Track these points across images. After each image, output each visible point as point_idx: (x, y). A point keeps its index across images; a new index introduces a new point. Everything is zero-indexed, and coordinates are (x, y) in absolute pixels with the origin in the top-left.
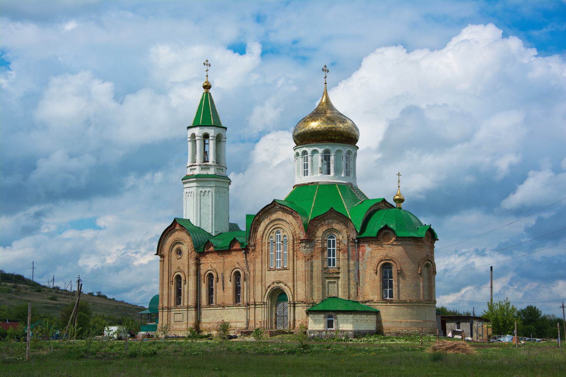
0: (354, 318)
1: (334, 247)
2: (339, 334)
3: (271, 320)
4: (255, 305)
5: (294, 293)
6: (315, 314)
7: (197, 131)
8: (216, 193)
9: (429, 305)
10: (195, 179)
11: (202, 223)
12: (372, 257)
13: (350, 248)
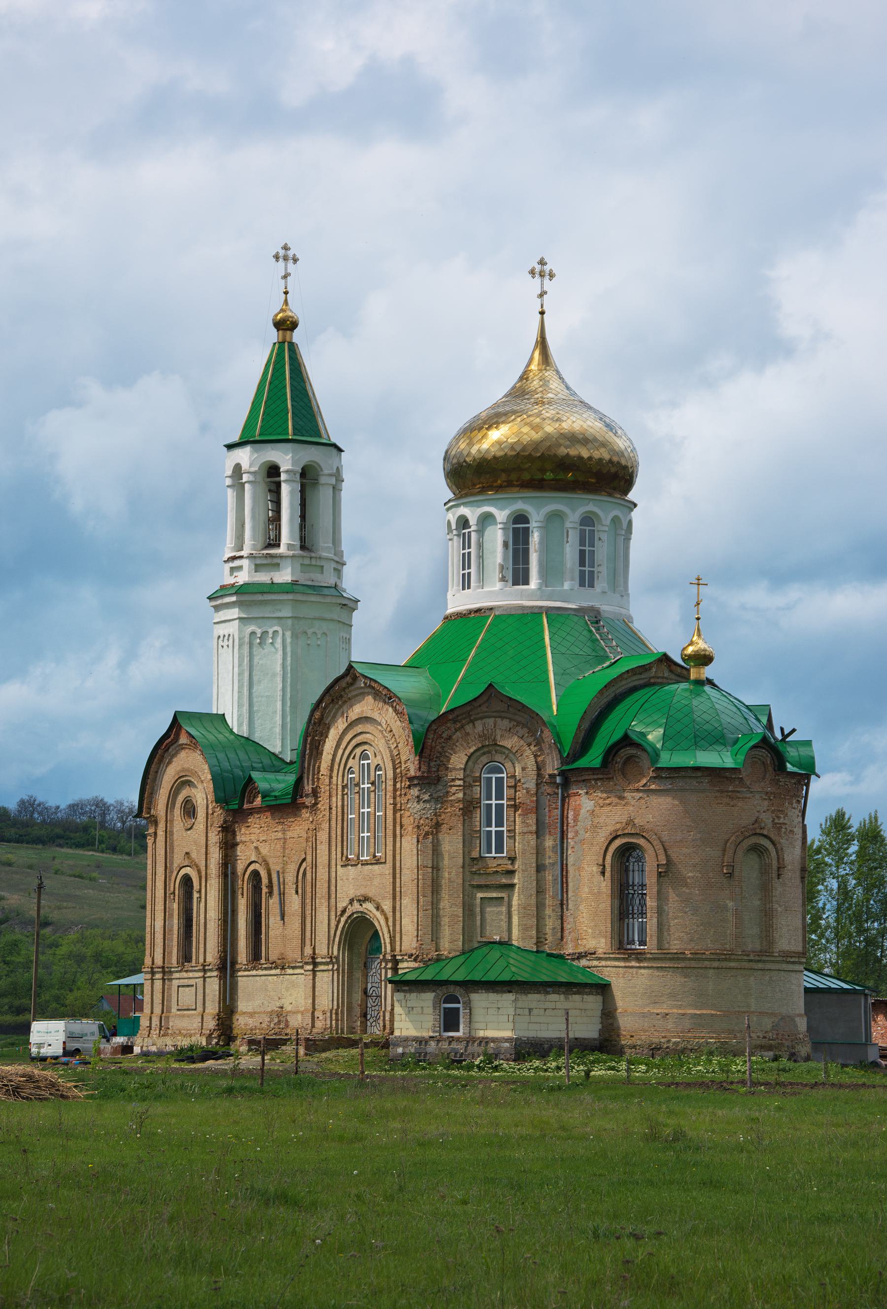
0: (520, 1004)
1: (500, 796)
2: (474, 1048)
3: (350, 1009)
4: (315, 964)
5: (394, 930)
6: (410, 991)
7: (244, 456)
8: (294, 636)
9: (760, 966)
10: (234, 599)
11: (257, 722)
12: (595, 827)
13: (545, 800)
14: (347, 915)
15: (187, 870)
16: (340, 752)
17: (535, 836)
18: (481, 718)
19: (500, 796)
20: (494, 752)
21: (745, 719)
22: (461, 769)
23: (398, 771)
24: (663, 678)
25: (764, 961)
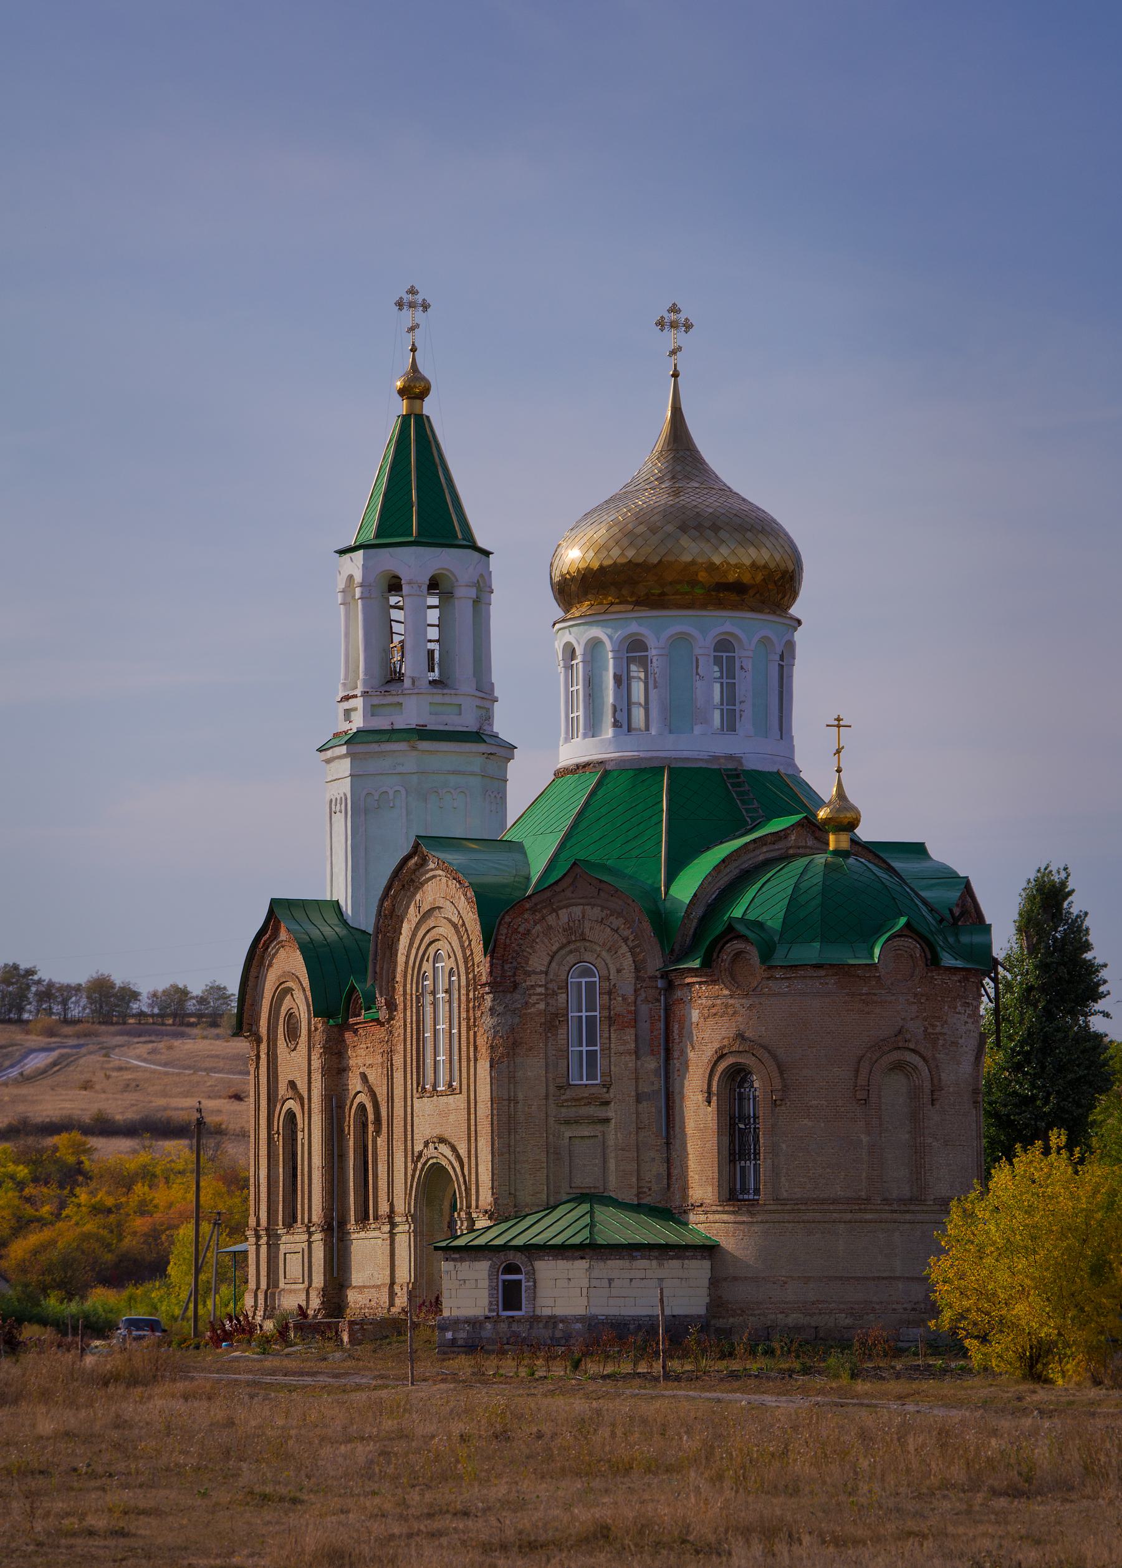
0: (596, 1273)
6: (462, 1260)
7: (354, 565)
9: (908, 1217)
14: (423, 1160)
15: (291, 1104)
16: (414, 951)
17: (634, 1057)
18: (567, 907)
19: (591, 1007)
20: (582, 950)
21: (894, 899)
22: (541, 972)
23: (471, 976)
24: (806, 847)
25: (913, 1212)
